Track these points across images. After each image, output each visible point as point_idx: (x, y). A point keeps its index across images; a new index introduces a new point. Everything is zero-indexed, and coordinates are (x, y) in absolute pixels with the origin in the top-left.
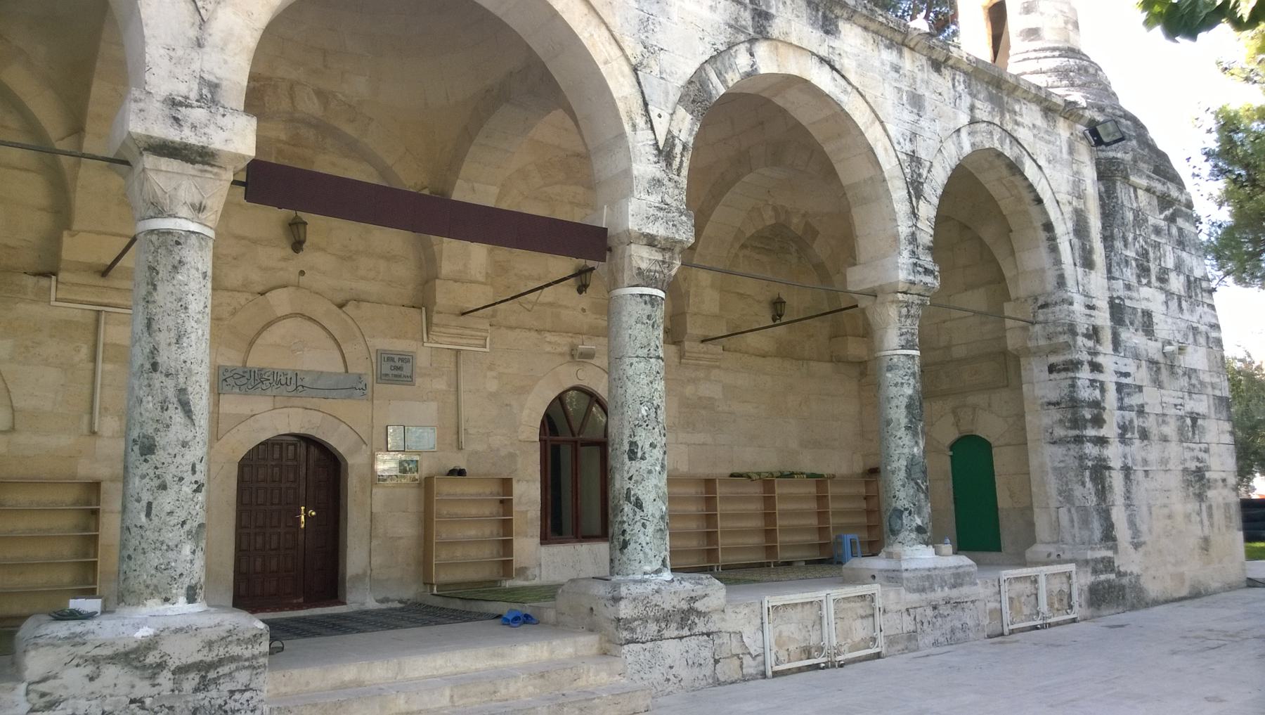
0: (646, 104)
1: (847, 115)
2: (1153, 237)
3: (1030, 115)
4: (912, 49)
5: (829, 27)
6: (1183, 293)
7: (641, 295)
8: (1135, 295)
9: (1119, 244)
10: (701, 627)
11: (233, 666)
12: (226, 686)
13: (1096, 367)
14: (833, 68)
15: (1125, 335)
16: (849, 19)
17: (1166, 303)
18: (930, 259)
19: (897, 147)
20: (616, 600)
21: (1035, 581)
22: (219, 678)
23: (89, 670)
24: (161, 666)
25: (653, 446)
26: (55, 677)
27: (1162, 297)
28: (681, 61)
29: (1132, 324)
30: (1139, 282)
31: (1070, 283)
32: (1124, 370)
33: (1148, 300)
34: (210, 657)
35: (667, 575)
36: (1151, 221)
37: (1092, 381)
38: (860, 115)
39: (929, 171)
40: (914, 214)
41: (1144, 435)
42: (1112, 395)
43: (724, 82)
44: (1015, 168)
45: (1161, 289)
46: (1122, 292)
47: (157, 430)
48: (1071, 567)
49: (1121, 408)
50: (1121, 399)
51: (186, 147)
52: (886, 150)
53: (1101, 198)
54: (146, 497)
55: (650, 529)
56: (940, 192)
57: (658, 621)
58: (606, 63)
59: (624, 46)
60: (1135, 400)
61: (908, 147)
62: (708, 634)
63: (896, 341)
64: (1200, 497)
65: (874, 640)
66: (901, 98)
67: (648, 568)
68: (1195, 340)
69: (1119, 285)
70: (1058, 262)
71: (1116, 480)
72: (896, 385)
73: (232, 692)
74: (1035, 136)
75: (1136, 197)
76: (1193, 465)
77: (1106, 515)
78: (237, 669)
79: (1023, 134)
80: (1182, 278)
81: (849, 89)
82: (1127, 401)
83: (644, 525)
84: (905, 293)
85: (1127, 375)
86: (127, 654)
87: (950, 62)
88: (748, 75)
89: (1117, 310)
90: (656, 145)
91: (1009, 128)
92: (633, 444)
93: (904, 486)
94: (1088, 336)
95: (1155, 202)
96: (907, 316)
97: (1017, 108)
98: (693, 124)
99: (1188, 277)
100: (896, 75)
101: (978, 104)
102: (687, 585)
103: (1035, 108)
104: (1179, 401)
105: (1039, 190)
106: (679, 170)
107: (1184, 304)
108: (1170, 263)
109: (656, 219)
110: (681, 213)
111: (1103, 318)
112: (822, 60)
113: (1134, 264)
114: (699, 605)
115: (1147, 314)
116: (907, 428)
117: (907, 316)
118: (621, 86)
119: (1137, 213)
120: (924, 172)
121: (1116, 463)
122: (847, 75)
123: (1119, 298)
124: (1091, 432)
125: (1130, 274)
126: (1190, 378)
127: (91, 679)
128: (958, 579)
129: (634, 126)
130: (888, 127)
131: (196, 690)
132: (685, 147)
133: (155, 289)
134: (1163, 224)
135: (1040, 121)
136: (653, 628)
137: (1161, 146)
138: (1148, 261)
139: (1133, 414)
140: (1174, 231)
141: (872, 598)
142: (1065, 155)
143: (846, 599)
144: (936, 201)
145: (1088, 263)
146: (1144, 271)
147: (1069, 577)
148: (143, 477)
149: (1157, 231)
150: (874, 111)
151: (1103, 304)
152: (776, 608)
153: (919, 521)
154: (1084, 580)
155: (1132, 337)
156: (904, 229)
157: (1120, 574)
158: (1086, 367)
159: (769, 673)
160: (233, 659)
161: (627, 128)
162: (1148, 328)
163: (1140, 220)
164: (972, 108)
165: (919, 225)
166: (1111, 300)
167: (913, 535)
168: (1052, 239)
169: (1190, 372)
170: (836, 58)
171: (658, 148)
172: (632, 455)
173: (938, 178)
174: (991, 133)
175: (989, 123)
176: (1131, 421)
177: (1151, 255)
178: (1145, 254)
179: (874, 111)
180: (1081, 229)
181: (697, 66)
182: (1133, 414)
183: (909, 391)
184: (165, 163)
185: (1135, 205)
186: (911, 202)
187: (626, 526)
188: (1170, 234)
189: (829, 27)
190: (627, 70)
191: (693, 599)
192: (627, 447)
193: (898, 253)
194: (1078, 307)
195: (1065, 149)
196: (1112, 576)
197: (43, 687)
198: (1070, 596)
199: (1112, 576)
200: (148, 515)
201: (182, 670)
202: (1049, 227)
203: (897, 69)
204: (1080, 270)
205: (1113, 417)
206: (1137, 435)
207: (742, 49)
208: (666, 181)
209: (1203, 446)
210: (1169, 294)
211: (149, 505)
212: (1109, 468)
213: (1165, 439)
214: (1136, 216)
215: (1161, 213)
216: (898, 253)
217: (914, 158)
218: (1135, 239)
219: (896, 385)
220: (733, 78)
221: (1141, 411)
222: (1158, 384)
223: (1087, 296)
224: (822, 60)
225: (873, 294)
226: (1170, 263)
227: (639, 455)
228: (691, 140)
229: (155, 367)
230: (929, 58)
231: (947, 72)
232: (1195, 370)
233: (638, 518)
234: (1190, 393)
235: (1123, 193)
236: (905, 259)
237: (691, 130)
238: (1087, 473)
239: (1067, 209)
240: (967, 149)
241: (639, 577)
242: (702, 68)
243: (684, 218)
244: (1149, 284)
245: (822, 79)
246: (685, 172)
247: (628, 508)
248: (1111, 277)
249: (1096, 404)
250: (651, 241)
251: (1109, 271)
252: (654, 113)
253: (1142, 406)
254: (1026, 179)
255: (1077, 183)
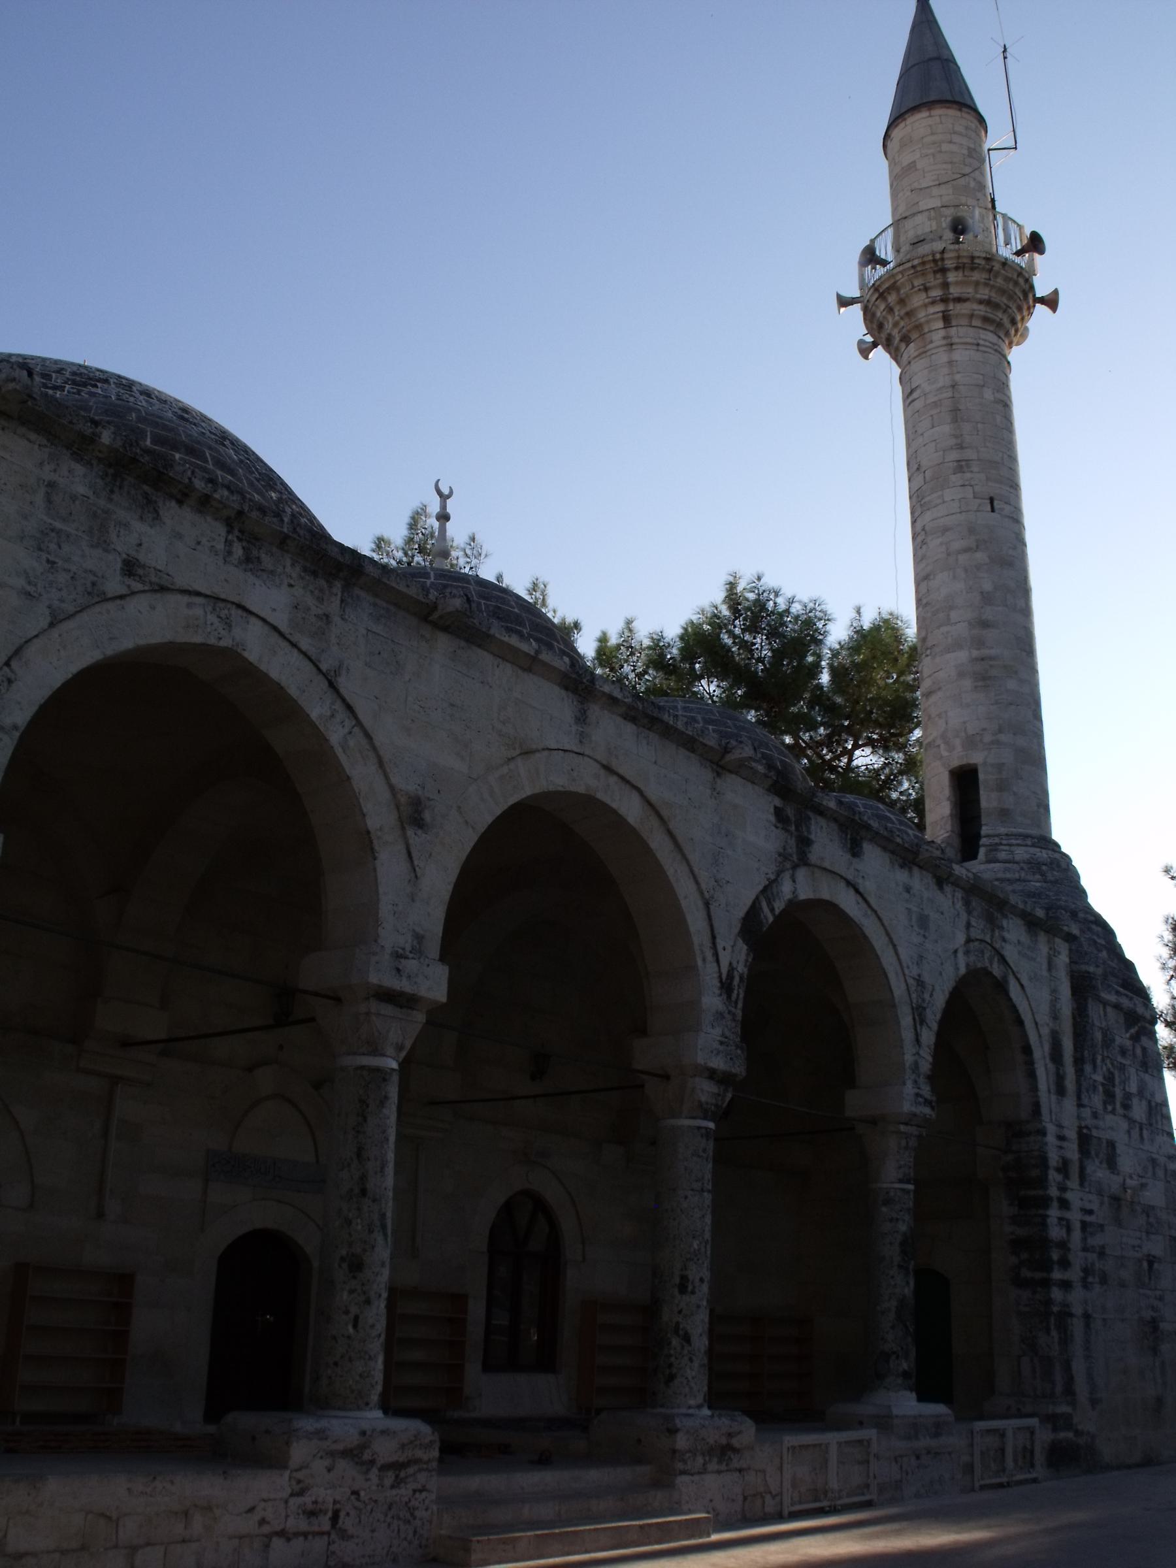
0: (714, 937)
1: (865, 937)
2: (1120, 1059)
3: (1014, 930)
4: (920, 867)
5: (855, 850)
6: (1144, 1121)
7: (699, 1128)
8: (1101, 1123)
9: (1088, 1068)
10: (735, 1464)
11: (416, 1467)
12: (412, 1486)
13: (1064, 1204)
14: (857, 891)
15: (1090, 1168)
16: (871, 840)
17: (1129, 1132)
18: (928, 1088)
19: (907, 972)
20: (673, 1431)
21: (1003, 1435)
22: (406, 1477)
23: (327, 1462)
24: (372, 1462)
25: (702, 1280)
26: (307, 1467)
27: (1124, 1125)
28: (741, 896)
29: (1097, 1155)
30: (1105, 1108)
31: (1045, 1111)
32: (1088, 1206)
33: (1112, 1128)
34: (402, 1458)
35: (706, 1412)
36: (1118, 1040)
37: (1061, 1219)
38: (878, 941)
39: (931, 995)
40: (918, 1041)
41: (1104, 1280)
42: (1077, 1235)
43: (772, 910)
44: (1001, 987)
45: (1125, 1116)
46: (1090, 1122)
47: (364, 1250)
48: (1034, 1422)
49: (1085, 1249)
50: (1084, 1239)
51: (402, 994)
52: (897, 974)
53: (1074, 1018)
54: (354, 1310)
55: (696, 1364)
56: (939, 1016)
57: (703, 1455)
58: (686, 897)
59: (700, 880)
60: (1096, 1241)
61: (915, 971)
62: (740, 1471)
63: (893, 1172)
64: (1155, 1351)
65: (867, 1486)
66: (910, 920)
67: (692, 1402)
68: (1154, 1173)
69: (1086, 1113)
70: (1034, 1089)
71: (1077, 1327)
72: (891, 1220)
73: (415, 1491)
74: (1019, 953)
75: (1105, 1015)
76: (1148, 1314)
77: (1067, 1367)
78: (420, 1470)
79: (1010, 952)
80: (1144, 1103)
81: (869, 912)
82: (1091, 1241)
83: (691, 1360)
84: (906, 1124)
85: (1090, 1212)
86: (351, 1450)
87: (952, 879)
88: (790, 901)
89: (1085, 1140)
90: (720, 977)
91: (997, 946)
92: (684, 1278)
93: (893, 1327)
94: (1058, 1170)
95: (1122, 1020)
96: (906, 1148)
97: (1005, 923)
98: (748, 955)
99: (1150, 1102)
100: (906, 895)
101: (973, 922)
102: (724, 1423)
103: (1020, 922)
104: (1138, 1242)
105: (1021, 1010)
106: (736, 1003)
107: (1145, 1132)
108: (1133, 1088)
109: (718, 1053)
110: (737, 1047)
111: (1072, 1151)
112: (849, 883)
113: (1101, 1088)
114: (735, 1442)
115: (1112, 1145)
116: (900, 1267)
117: (906, 1148)
118: (696, 922)
119: (1105, 1032)
120: (927, 996)
121: (1078, 1310)
122: (869, 899)
123: (1086, 1127)
124: (1057, 1275)
125: (1097, 1100)
126: (1148, 1216)
127: (329, 1471)
128: (938, 1429)
129: (704, 960)
130: (900, 950)
131: (392, 1487)
132: (741, 977)
133: (365, 1121)
134: (1128, 1043)
135: (1025, 938)
136: (700, 1460)
137: (1129, 954)
138: (1114, 1086)
139: (1095, 1256)
140: (1139, 1051)
141: (869, 1441)
142: (1045, 973)
143: (847, 1443)
144: (935, 1026)
145: (1061, 1091)
146: (1109, 1096)
147: (1032, 1433)
148: (351, 1292)
149: (1123, 1052)
150: (888, 934)
151: (1072, 1134)
152: (794, 1448)
153: (905, 1366)
154: (1044, 1436)
155: (1098, 1172)
156: (909, 1058)
157: (1078, 1433)
158: (1055, 1204)
159: (786, 1513)
160: (417, 1461)
161: (700, 963)
162: (1111, 1163)
163: (1108, 1042)
164: (968, 925)
165: (921, 1052)
166: (1080, 1128)
167: (900, 1381)
168: (1030, 1063)
169: (1148, 1210)
170: (860, 881)
171: (721, 981)
172: (683, 1288)
173: (939, 1000)
174: (982, 952)
175: (981, 941)
176: (1093, 1264)
177: (1117, 1081)
178: (1110, 1078)
179: (888, 934)
180: (1056, 1055)
181: (753, 897)
182: (1095, 1256)
183: (903, 1228)
184: (388, 1009)
185: (1104, 1024)
186: (916, 1029)
187: (673, 1359)
188: (1134, 1055)
189: (855, 850)
190: (700, 904)
191: (730, 1435)
192: (677, 1280)
193: (902, 1080)
194: (1051, 1139)
195: (1045, 966)
196: (1070, 1435)
197: (299, 1475)
198: (1032, 1452)
199: (1070, 1435)
200: (355, 1326)
201: (385, 1468)
202: (1027, 1050)
203: (908, 890)
204: (1054, 1097)
205: (1078, 1259)
206: (1097, 1279)
207: (787, 876)
208: (727, 1016)
209: (1158, 1293)
210: (1131, 1121)
211: (356, 1318)
212: (1071, 1315)
213: (1123, 1285)
214: (1105, 1035)
215: (1127, 1031)
216: (902, 1080)
217: (920, 983)
218: (1103, 1060)
219: (891, 1220)
220: (779, 906)
221: (1102, 1254)
222: (1118, 1222)
223: (1060, 1126)
224: (849, 883)
225: (873, 1122)
226: (1133, 1088)
227: (690, 1288)
228: (746, 970)
229: (364, 1192)
230: (935, 876)
231: (948, 889)
232: (1153, 1208)
233: (685, 1352)
234: (1148, 1233)
235: (1095, 1012)
236: (909, 1089)
237: (747, 961)
238: (1052, 1320)
239: (1045, 1031)
240: (963, 970)
241: (684, 1410)
242: (757, 898)
243: (739, 1052)
244: (1113, 1112)
245: (848, 902)
246: (740, 1005)
247: (675, 1342)
248: (1080, 1105)
249: (1063, 1245)
250: (711, 1074)
251: (1079, 1098)
252: (720, 944)
253: (1103, 1247)
254: (1010, 999)
255: (1054, 1002)
